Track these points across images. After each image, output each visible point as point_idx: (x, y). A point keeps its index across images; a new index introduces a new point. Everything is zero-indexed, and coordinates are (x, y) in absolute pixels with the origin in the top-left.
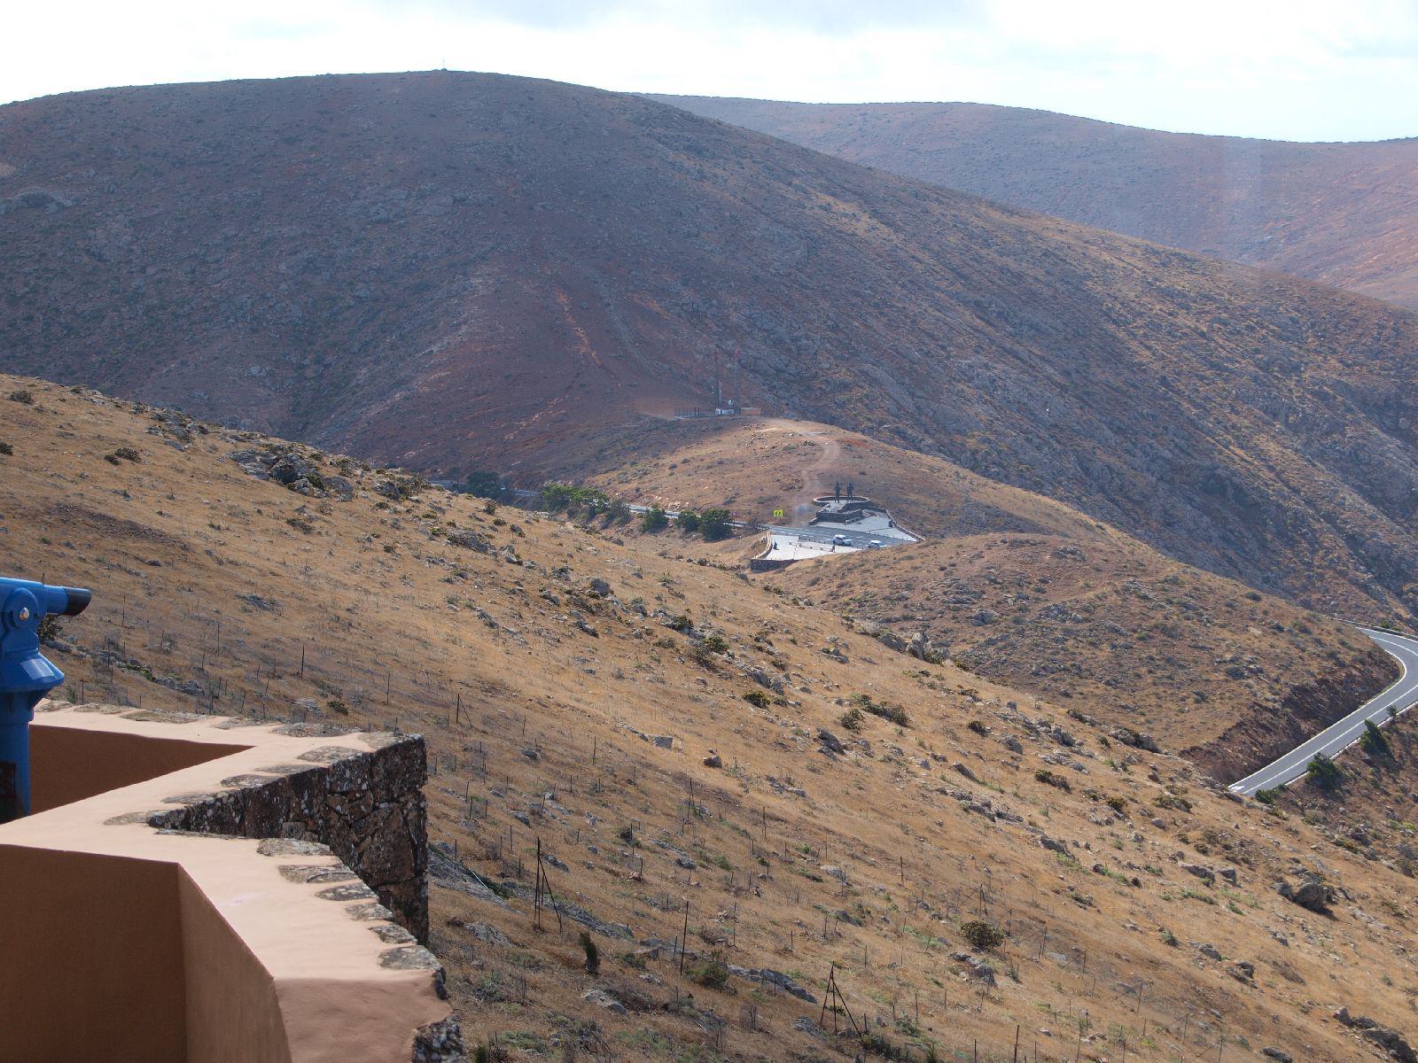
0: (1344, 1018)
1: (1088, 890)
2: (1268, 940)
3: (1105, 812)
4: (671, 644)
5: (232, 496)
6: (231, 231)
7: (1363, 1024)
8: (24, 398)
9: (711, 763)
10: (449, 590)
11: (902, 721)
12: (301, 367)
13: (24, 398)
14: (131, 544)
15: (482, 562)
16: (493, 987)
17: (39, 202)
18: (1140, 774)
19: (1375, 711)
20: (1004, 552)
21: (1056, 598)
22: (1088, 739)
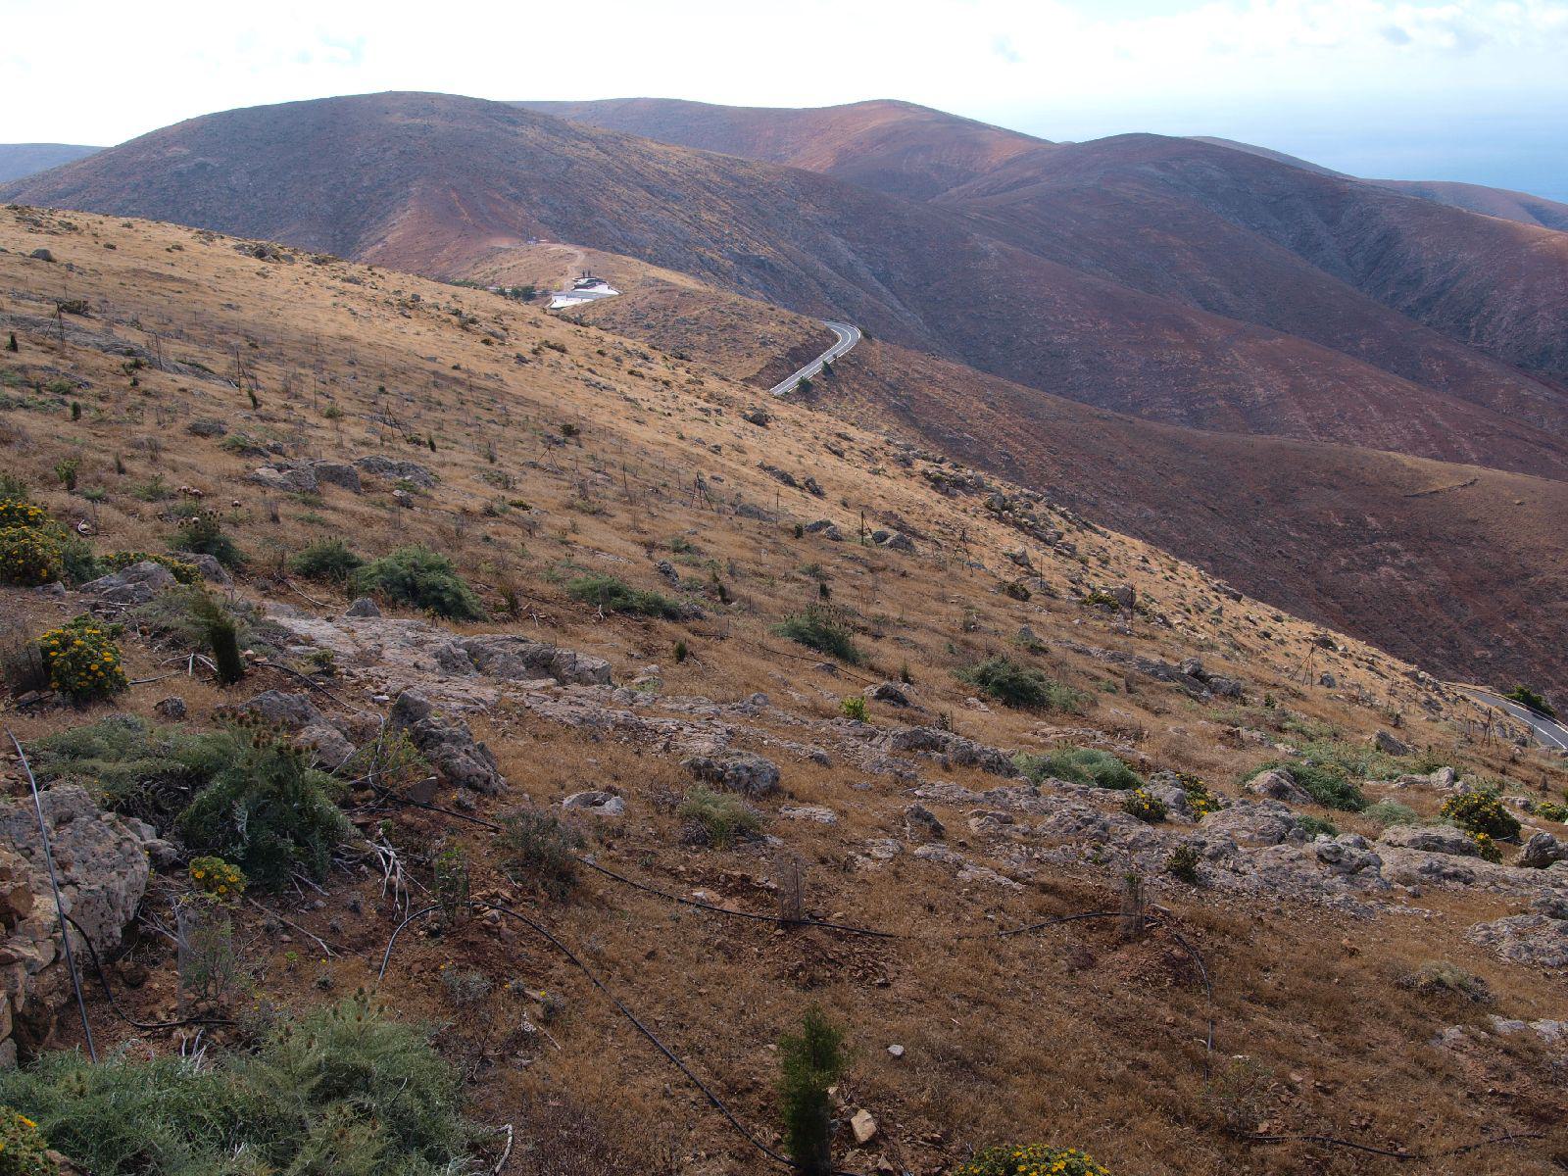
0: (761, 466)
1: (643, 417)
2: (732, 437)
3: (660, 386)
4: (449, 321)
6: (295, 173)
7: (770, 469)
8: (129, 226)
9: (455, 368)
10: (335, 300)
12: (334, 236)
13: (129, 226)
14: (170, 285)
15: (357, 288)
17: (203, 166)
18: (681, 371)
19: (827, 357)
20: (656, 295)
21: (682, 314)
22: (657, 356)
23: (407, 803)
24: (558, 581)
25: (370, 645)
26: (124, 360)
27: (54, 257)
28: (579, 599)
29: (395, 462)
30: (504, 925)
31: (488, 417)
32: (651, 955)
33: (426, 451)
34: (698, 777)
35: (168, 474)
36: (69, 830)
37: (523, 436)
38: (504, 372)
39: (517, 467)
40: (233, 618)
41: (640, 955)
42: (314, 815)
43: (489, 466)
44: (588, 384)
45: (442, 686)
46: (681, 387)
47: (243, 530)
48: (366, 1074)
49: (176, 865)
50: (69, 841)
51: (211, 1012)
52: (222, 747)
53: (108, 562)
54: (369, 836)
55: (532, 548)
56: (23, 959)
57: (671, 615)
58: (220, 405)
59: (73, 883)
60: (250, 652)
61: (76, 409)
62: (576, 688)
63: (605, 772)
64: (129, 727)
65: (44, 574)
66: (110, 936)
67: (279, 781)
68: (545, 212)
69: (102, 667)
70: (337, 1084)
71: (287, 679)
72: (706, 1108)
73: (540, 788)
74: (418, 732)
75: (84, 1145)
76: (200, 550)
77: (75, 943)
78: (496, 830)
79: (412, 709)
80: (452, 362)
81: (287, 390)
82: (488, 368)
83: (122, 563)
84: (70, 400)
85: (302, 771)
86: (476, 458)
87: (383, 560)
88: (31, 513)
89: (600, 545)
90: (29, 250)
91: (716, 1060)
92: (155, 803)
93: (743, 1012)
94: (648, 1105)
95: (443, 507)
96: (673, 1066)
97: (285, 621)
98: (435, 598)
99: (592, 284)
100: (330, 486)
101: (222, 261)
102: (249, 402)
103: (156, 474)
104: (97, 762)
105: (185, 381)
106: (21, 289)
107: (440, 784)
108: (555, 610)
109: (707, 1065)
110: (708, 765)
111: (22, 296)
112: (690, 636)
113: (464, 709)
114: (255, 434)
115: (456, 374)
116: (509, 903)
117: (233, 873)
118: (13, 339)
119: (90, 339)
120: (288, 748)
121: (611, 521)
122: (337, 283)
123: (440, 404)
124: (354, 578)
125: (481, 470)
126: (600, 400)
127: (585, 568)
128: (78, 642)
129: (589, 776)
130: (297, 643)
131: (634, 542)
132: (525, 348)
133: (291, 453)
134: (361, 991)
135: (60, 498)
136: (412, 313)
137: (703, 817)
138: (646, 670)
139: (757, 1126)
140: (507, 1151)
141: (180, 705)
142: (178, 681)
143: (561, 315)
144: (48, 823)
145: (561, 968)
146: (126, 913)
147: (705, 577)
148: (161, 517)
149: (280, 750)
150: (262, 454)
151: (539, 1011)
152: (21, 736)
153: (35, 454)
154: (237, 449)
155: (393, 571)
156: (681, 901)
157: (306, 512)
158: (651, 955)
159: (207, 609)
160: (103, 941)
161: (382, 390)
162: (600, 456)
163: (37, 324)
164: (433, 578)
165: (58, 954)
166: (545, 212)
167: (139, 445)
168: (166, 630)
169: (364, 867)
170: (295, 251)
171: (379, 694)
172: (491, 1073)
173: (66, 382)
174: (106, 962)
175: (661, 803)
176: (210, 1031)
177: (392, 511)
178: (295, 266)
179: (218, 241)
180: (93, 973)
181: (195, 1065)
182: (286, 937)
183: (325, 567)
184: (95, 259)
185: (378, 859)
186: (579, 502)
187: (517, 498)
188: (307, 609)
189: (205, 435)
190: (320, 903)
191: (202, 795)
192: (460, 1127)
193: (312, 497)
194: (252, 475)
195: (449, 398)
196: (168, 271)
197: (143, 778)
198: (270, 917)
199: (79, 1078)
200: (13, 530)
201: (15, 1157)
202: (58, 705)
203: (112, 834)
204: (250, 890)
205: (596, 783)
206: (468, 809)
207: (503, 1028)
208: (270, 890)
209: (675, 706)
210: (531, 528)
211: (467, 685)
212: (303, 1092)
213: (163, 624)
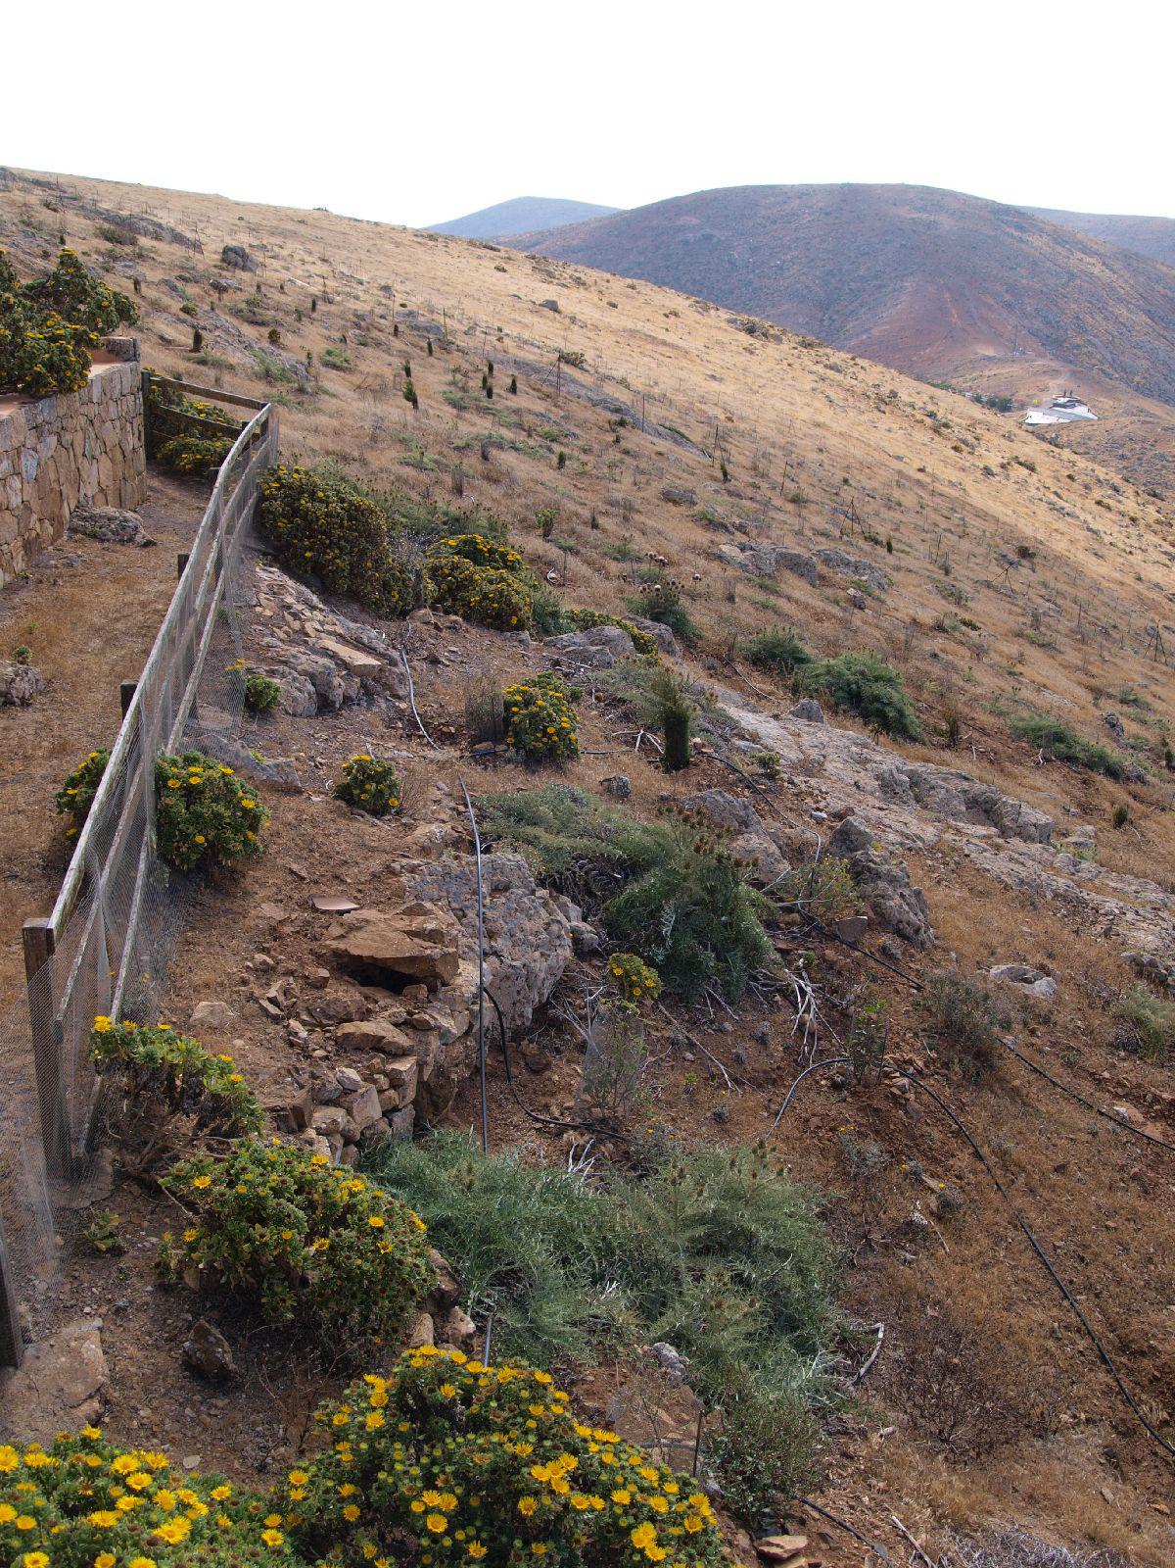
1: (1104, 551)
3: (1126, 521)
5: (720, 336)
8: (633, 287)
9: (920, 470)
10: (814, 385)
11: (1032, 469)
12: (822, 320)
14: (661, 349)
15: (838, 377)
16: (1032, 718)
17: (709, 237)
18: (1151, 509)
20: (1139, 425)
22: (1129, 490)
23: (833, 937)
24: (1000, 714)
25: (814, 754)
26: (609, 415)
27: (560, 308)
28: (1019, 738)
29: (852, 559)
30: (912, 1096)
31: (944, 524)
32: (1060, 1169)
33: (882, 551)
34: (1139, 974)
35: (637, 535)
36: (503, 900)
37: (979, 551)
38: (968, 481)
39: (970, 583)
40: (687, 701)
41: (1048, 1166)
42: (739, 932)
43: (942, 578)
44: (1053, 507)
45: (882, 813)
46: (1148, 526)
47: (699, 605)
48: (750, 1237)
49: (594, 953)
50: (502, 910)
51: (603, 1121)
52: (661, 841)
53: (573, 618)
54: (789, 964)
55: (978, 675)
56: (439, 1028)
57: (1113, 773)
58: (693, 474)
59: (497, 954)
60: (698, 740)
61: (562, 458)
62: (1016, 842)
63: (1038, 946)
64: (575, 800)
65: (514, 620)
66: (522, 1015)
67: (712, 891)
68: (1038, 324)
69: (560, 732)
70: (720, 1241)
71: (731, 777)
72: (1093, 1363)
73: (967, 950)
74: (855, 863)
75: (463, 1244)
76: (657, 618)
77: (489, 1017)
78: (919, 988)
79: (853, 838)
80: (918, 464)
81: (755, 468)
82: (953, 475)
83: (587, 623)
84: (557, 448)
85: (737, 884)
86: (931, 567)
87: (832, 662)
88: (510, 557)
89: (1047, 682)
90: (540, 298)
91: (1114, 1309)
92: (586, 883)
93: (1150, 1260)
94: (1032, 1342)
95: (895, 614)
96: (1066, 1303)
97: (733, 712)
98: (877, 710)
99: (1071, 404)
100: (788, 575)
101: (714, 332)
102: (720, 475)
103: (627, 535)
104: (539, 831)
105: (663, 445)
106: (526, 335)
107: (870, 924)
108: (997, 745)
109: (1103, 1312)
110: (1152, 964)
111: (525, 342)
112: (1131, 801)
113: (901, 844)
114: (721, 509)
115: (920, 476)
116: (920, 1072)
117: (651, 978)
118: (514, 382)
119: (583, 392)
120: (729, 858)
121: (1060, 657)
122: (819, 368)
123: (900, 505)
124: (800, 673)
125: (934, 580)
126: (1061, 525)
127: (1029, 705)
128: (540, 702)
129: (1021, 945)
130: (743, 738)
131: (1080, 684)
132: (994, 461)
133: (754, 533)
134: (761, 1145)
135: (535, 544)
136: (887, 409)
137: (1139, 1022)
138: (1083, 830)
139: (1144, 1397)
140: (875, 1353)
141: (625, 785)
142: (624, 758)
143: (1038, 433)
144: (484, 889)
145: (963, 1160)
146: (541, 995)
147: (1151, 736)
148: (624, 578)
149: (720, 859)
150: (727, 529)
151: (933, 1202)
152: (472, 787)
153: (519, 496)
154: (704, 522)
155: (840, 675)
156: (1102, 1114)
157: (761, 597)
158: (1060, 1169)
159: (667, 692)
160: (513, 1019)
161: (846, 481)
162: (1052, 584)
163: (538, 371)
164: (878, 689)
165: (471, 1026)
166: (1038, 324)
167: (613, 503)
168: (623, 701)
169: (778, 998)
170: (784, 332)
171: (817, 809)
172: (872, 1259)
173: (555, 430)
174: (513, 1040)
175: (1094, 998)
176: (601, 1141)
177: (844, 610)
178: (781, 347)
179: (712, 312)
180: (499, 1048)
181: (576, 1174)
182: (689, 1056)
183: (773, 657)
184: (597, 315)
185: (794, 991)
186: (1029, 632)
187: (967, 617)
188: (756, 701)
189: (675, 503)
190: (728, 1026)
191: (633, 888)
192: (835, 1316)
193: (768, 582)
194: (715, 551)
195: (909, 499)
196: (662, 335)
197: (581, 857)
198: (677, 1031)
199: (470, 1170)
200: (492, 572)
201: (401, 1262)
202: (509, 761)
203: (543, 912)
204: (664, 996)
205: (1028, 957)
206: (891, 957)
207: (893, 1213)
208: (681, 1000)
209: (1119, 885)
210: (979, 652)
211: (906, 817)
212: (682, 1240)
213: (619, 695)
